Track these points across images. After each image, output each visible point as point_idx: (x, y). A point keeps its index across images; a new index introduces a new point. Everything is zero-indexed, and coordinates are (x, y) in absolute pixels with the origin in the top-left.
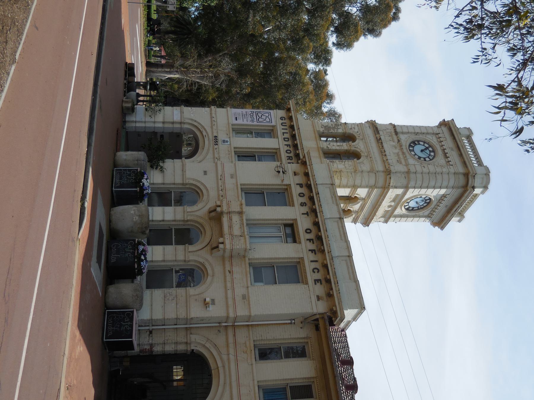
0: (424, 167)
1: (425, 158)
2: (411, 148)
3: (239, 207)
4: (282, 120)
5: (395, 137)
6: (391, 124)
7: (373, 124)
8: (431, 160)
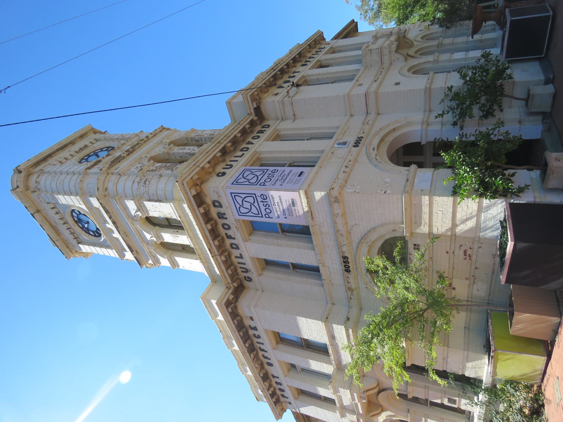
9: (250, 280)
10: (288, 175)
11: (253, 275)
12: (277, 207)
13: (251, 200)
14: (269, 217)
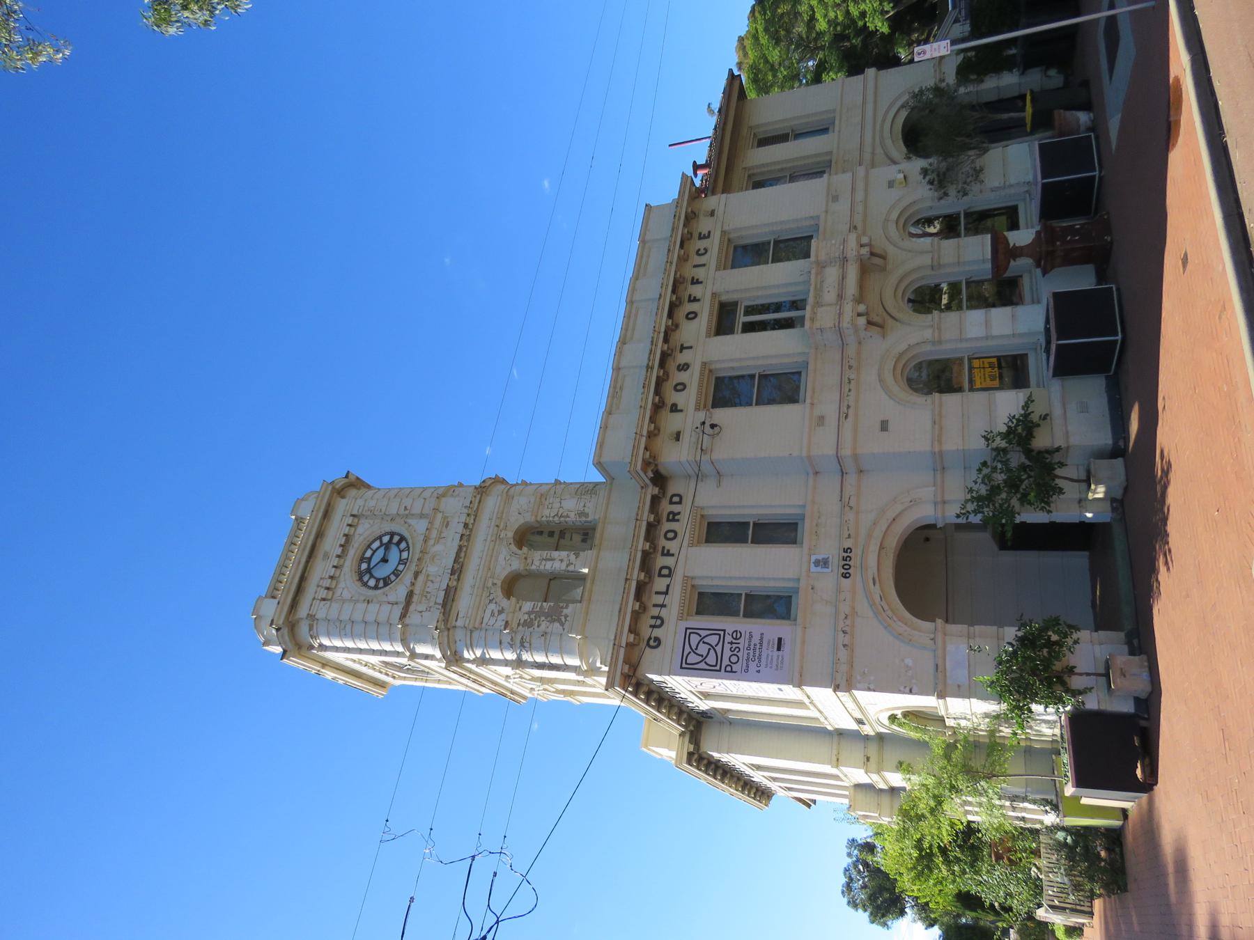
0: (406, 508)
3: (819, 315)
4: (657, 640)
5: (417, 590)
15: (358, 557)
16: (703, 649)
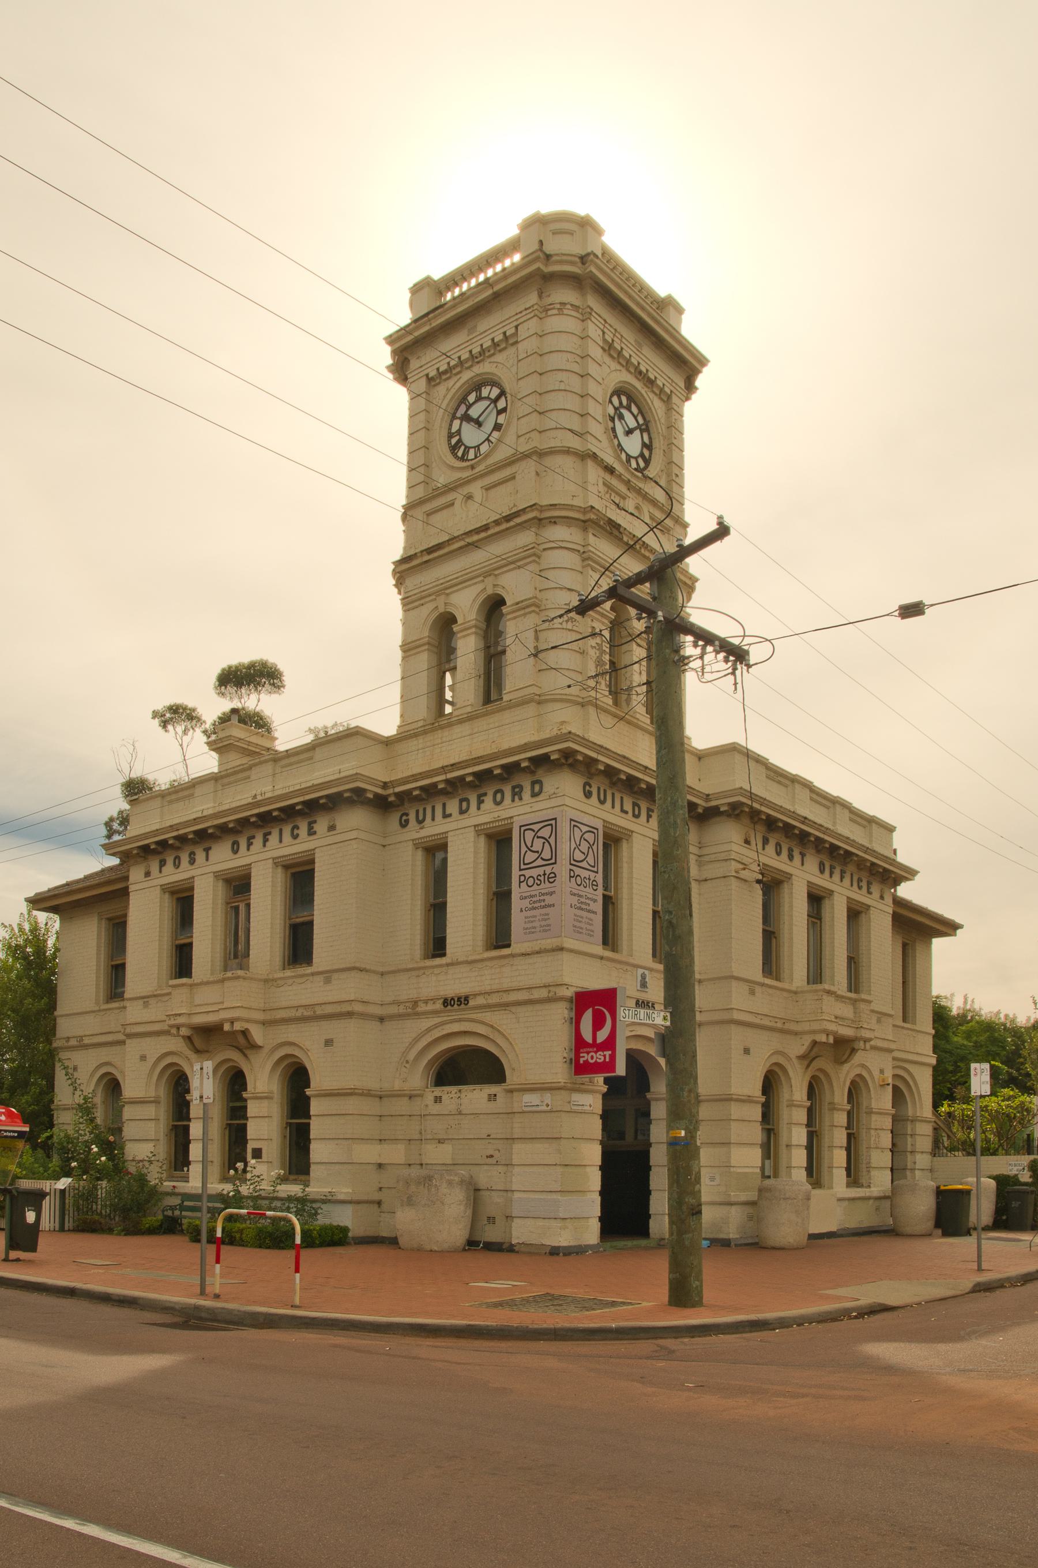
1: (500, 412)
2: (471, 454)
4: (407, 821)
6: (405, 517)
7: (406, 569)
8: (503, 393)
9: (404, 824)
10: (589, 911)
11: (414, 832)
12: (538, 898)
13: (546, 854)
14: (520, 882)
15: (444, 433)
16: (538, 845)
